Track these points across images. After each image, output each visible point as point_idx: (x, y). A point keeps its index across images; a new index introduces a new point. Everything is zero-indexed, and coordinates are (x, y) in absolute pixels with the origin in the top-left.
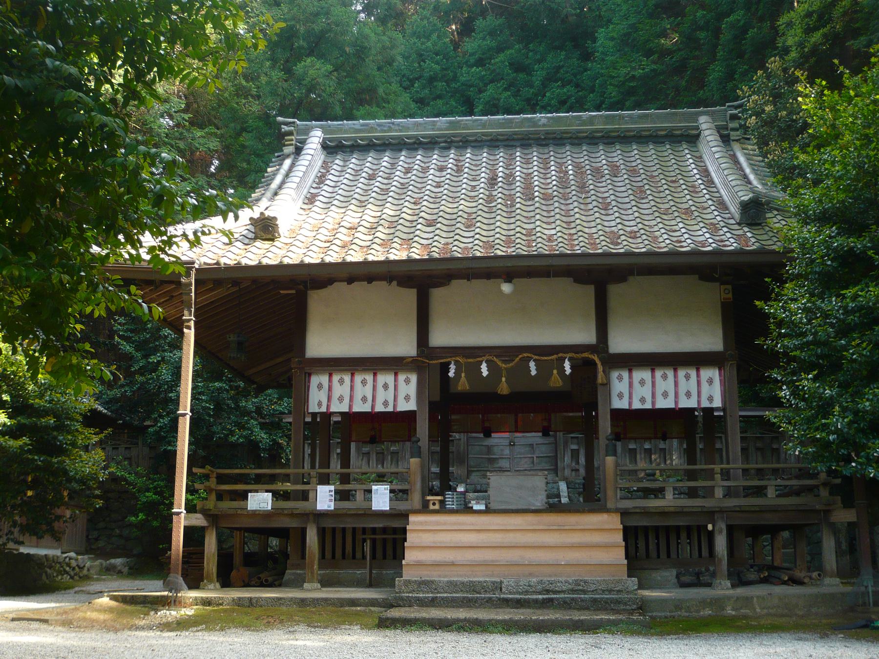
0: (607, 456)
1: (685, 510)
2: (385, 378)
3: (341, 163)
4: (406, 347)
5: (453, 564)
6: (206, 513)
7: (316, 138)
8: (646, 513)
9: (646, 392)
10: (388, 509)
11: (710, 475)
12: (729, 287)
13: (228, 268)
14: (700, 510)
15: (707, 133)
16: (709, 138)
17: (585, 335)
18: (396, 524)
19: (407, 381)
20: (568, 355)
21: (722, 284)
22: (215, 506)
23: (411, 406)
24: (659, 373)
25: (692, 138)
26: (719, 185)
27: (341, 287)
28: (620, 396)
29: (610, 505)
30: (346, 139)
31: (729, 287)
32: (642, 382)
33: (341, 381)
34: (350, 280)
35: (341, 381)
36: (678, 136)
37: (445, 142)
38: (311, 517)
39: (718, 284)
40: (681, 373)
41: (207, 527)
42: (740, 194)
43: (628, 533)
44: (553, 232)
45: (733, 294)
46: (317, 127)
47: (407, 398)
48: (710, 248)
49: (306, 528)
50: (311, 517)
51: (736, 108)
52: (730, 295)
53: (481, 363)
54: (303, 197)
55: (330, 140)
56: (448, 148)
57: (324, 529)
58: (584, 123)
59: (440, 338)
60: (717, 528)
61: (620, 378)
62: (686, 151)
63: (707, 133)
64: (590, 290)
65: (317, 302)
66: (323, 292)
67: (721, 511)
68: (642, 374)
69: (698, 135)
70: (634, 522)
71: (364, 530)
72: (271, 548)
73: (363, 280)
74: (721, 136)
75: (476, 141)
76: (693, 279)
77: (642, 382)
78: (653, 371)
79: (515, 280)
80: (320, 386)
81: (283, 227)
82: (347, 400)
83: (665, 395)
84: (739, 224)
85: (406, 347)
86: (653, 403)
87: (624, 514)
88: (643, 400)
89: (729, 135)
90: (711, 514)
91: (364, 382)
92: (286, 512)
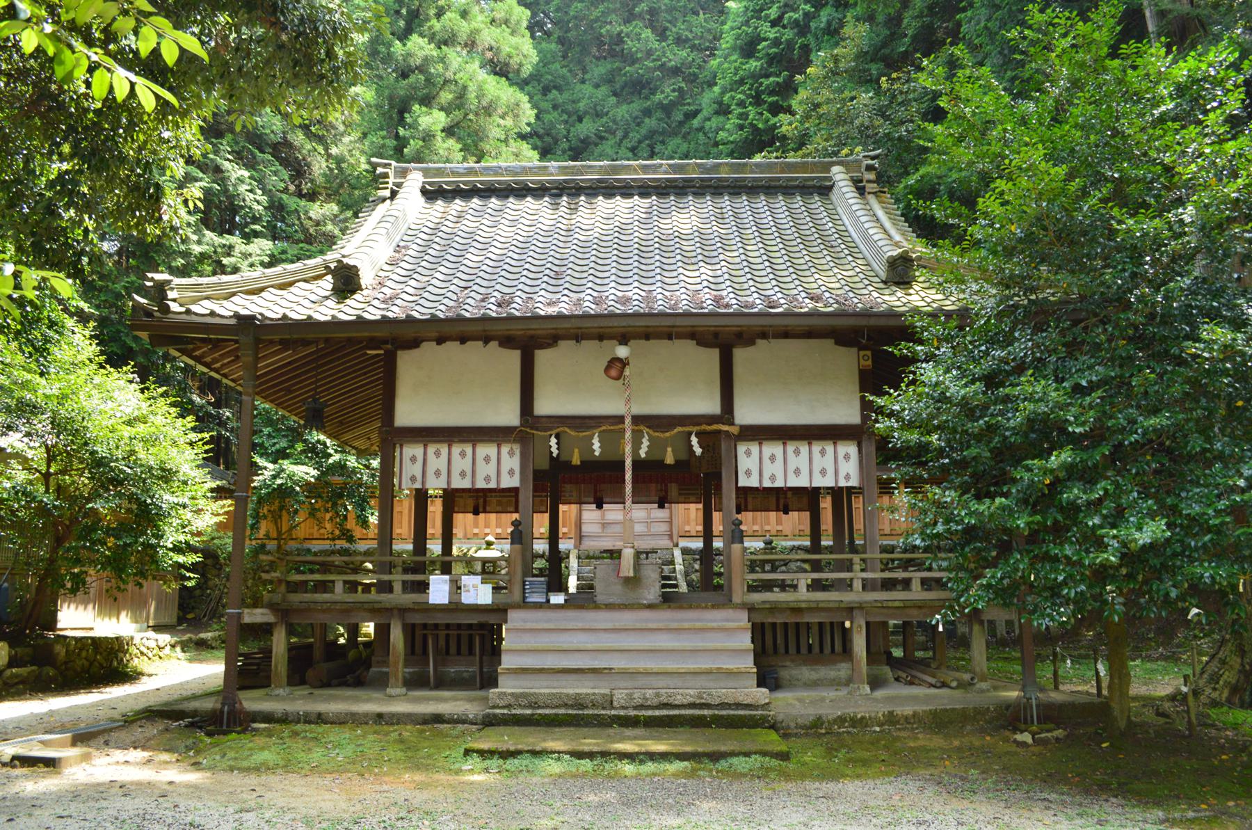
0: (733, 543)
1: (821, 605)
2: (487, 450)
3: (442, 210)
4: (509, 415)
5: (648, 673)
6: (272, 607)
7: (415, 180)
8: (774, 608)
9: (491, 469)
10: (446, 601)
11: (848, 567)
12: (869, 353)
13: (298, 324)
14: (836, 605)
15: (841, 184)
16: (844, 190)
17: (706, 403)
18: (492, 619)
19: (511, 454)
20: (554, 432)
21: (860, 349)
22: (284, 600)
23: (514, 482)
24: (431, 449)
25: (825, 190)
26: (857, 240)
27: (428, 348)
28: (748, 473)
29: (737, 599)
30: (447, 183)
31: (869, 353)
32: (487, 459)
33: (438, 454)
34: (463, 340)
35: (438, 454)
36: (809, 187)
37: (557, 188)
38: (395, 612)
39: (855, 350)
40: (456, 449)
41: (276, 624)
42: (885, 249)
43: (759, 632)
44: (699, 287)
45: (873, 361)
46: (415, 169)
47: (511, 472)
48: (831, 309)
49: (389, 625)
50: (395, 612)
51: (873, 158)
52: (870, 362)
53: (592, 437)
54: (394, 244)
55: (430, 184)
56: (560, 196)
57: (413, 625)
58: (708, 171)
59: (545, 406)
60: (855, 625)
61: (748, 453)
62: (816, 202)
63: (841, 184)
64: (714, 355)
65: (407, 364)
66: (414, 353)
67: (861, 607)
68: (773, 449)
69: (831, 187)
70: (759, 618)
71: (425, 626)
72: (9, 624)
73: (455, 340)
74: (858, 188)
75: (590, 188)
76: (829, 343)
77: (773, 458)
78: (499, 446)
79: (632, 342)
80: (413, 459)
81: (366, 278)
82: (830, 471)
83: (823, 472)
84: (885, 282)
85: (509, 415)
86: (498, 482)
87: (751, 609)
88: (773, 478)
89: (864, 187)
90: (850, 610)
91: (463, 454)
92: (366, 606)
